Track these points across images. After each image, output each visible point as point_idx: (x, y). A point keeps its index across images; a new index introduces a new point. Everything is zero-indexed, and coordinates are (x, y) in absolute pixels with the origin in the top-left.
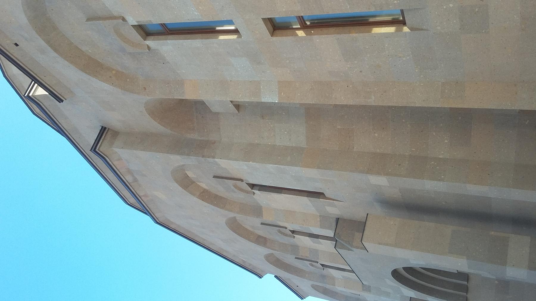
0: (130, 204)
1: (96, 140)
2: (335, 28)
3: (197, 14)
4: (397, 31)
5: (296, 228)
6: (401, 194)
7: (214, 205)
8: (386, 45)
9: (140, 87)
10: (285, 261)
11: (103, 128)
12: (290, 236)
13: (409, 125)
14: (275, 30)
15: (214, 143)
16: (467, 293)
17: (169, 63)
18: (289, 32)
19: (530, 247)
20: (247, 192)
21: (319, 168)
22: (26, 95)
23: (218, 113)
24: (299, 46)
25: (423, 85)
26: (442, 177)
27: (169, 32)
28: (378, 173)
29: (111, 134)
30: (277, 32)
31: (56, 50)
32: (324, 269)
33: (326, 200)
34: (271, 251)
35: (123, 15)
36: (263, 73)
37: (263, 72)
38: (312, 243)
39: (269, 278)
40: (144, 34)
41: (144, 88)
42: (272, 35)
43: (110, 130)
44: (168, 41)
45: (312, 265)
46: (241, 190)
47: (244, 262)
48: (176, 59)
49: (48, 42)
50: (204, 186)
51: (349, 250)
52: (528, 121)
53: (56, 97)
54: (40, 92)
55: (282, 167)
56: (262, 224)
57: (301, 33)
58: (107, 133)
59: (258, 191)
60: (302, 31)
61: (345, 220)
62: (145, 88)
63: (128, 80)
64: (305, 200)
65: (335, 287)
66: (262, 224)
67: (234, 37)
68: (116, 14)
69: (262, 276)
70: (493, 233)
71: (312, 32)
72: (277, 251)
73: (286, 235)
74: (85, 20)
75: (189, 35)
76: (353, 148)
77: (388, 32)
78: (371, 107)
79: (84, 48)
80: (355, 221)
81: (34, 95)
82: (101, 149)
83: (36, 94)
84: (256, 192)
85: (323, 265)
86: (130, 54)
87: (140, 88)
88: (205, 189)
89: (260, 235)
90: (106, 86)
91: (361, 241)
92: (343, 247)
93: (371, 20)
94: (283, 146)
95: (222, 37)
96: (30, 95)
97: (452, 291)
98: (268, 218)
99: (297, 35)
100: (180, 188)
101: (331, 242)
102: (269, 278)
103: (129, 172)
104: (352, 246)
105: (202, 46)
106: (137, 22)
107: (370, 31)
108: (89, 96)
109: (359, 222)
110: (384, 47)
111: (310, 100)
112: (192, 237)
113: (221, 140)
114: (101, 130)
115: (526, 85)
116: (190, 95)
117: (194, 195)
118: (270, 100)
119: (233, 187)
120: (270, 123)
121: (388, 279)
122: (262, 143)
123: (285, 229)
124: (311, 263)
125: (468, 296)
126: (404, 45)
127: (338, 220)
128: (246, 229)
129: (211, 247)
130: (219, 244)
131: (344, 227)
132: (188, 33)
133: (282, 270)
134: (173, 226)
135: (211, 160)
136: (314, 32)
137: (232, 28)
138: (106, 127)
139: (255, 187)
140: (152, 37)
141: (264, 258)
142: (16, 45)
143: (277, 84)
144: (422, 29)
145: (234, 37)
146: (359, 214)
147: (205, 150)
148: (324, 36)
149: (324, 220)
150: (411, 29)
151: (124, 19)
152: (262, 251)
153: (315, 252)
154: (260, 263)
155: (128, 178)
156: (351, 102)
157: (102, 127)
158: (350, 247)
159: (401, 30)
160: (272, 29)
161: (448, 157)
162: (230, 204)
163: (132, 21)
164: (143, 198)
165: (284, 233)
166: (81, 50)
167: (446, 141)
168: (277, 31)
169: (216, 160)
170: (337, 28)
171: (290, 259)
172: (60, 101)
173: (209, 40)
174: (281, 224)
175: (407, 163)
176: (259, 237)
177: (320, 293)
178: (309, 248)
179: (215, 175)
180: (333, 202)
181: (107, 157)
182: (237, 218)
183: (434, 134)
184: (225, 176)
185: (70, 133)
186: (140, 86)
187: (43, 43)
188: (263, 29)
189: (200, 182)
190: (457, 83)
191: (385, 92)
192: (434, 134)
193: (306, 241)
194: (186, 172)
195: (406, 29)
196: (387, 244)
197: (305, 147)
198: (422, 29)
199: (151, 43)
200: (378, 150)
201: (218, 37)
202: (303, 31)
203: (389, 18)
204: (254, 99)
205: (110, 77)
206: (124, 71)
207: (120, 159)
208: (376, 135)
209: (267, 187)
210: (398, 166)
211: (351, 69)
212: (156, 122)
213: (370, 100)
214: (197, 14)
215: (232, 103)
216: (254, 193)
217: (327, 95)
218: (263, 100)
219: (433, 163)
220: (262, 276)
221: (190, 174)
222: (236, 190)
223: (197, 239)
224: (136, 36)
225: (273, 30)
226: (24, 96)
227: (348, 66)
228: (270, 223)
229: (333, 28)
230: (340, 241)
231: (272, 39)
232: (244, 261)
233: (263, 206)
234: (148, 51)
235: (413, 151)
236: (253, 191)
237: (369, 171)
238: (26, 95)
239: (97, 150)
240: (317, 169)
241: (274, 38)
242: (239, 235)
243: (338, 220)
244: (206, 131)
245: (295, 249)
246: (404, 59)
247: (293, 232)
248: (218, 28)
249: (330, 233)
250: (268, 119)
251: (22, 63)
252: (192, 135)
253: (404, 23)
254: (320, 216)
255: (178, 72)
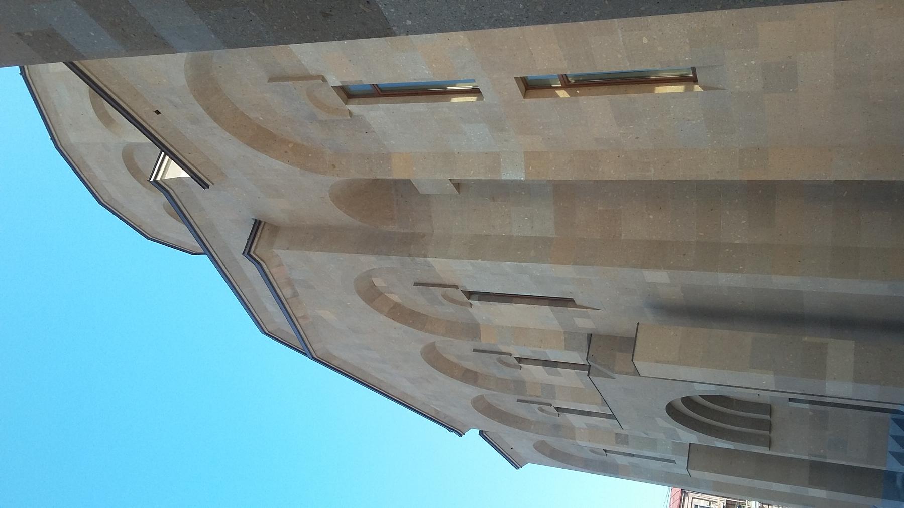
0: (267, 333)
1: (248, 240)
2: (607, 87)
3: (427, 73)
4: (686, 90)
5: (527, 352)
6: (683, 294)
7: (410, 325)
8: (672, 107)
9: (327, 164)
10: (500, 408)
11: (258, 222)
12: (515, 366)
13: (694, 203)
14: (529, 89)
15: (424, 236)
16: (770, 431)
17: (375, 133)
18: (546, 91)
19: (855, 354)
20: (461, 304)
21: (576, 264)
22: (152, 179)
23: (429, 195)
24: (559, 109)
25: (716, 153)
26: (741, 267)
27: (381, 94)
28: (657, 267)
29: (269, 230)
30: (531, 92)
31: (216, 119)
32: (559, 414)
33: (577, 309)
34: (483, 392)
35: (323, 74)
36: (505, 143)
37: (505, 141)
38: (547, 375)
39: (473, 434)
40: (345, 96)
41: (333, 165)
42: (525, 97)
43: (266, 225)
44: (379, 105)
45: (542, 410)
46: (453, 301)
47: (438, 412)
48: (386, 127)
49: (207, 109)
50: (395, 298)
51: (608, 378)
52: (846, 192)
53: (201, 182)
54: (173, 171)
55: (524, 264)
56: (475, 350)
57: (562, 94)
58: (263, 228)
59: (477, 302)
60: (564, 91)
61: (600, 336)
62: (334, 166)
63: (310, 155)
64: (545, 310)
65: (574, 441)
66: (475, 350)
67: (473, 99)
68: (313, 72)
69: (462, 433)
70: (806, 338)
71: (578, 92)
72: (494, 391)
73: (509, 365)
74: (267, 81)
75: (410, 97)
76: (621, 235)
77: (675, 92)
78: (651, 182)
79: (252, 115)
80: (615, 337)
81: (163, 179)
82: (257, 253)
83: (165, 178)
84: (475, 303)
85: (558, 409)
86: (321, 121)
87: (327, 166)
88: (396, 303)
89: (468, 368)
90: (278, 165)
91: (632, 360)
92: (600, 374)
93: (653, 77)
94: (523, 236)
95: (455, 100)
96: (158, 178)
97: (750, 430)
98: (485, 341)
99: (558, 96)
100: (363, 303)
101: (576, 372)
102: (473, 434)
103: (290, 283)
104: (613, 371)
105: (427, 110)
106: (341, 82)
107: (652, 91)
108: (248, 179)
109: (621, 337)
110: (669, 108)
111: (568, 174)
112: (359, 375)
113: (433, 231)
114: (254, 225)
115: (842, 150)
116: (398, 173)
117: (381, 312)
118: (514, 177)
119: (441, 298)
120: (504, 206)
121: (661, 418)
122: (492, 234)
123: (509, 356)
124: (541, 407)
125: (772, 435)
126: (694, 106)
127: (590, 337)
128: (449, 360)
129: (391, 391)
130: (405, 387)
131: (600, 346)
132: (408, 95)
133: (496, 421)
134: (335, 363)
135: (422, 259)
136: (579, 92)
137: (469, 87)
138: (261, 220)
139: (473, 297)
140: (356, 100)
141: (471, 404)
142: (158, 112)
143: (523, 156)
144: (717, 89)
145: (471, 99)
146: (623, 326)
147: (412, 246)
148: (593, 97)
149: (570, 338)
150: (704, 88)
151: (324, 80)
152: (471, 391)
153: (550, 389)
154: (454, 413)
155: (286, 293)
156: (623, 177)
157: (256, 220)
158: (609, 373)
159: (692, 90)
160: (524, 88)
161: (747, 242)
162: (432, 322)
163: (334, 80)
164: (300, 321)
165: (506, 363)
166: (249, 118)
167: (744, 222)
168: (531, 90)
169: (429, 259)
170: (610, 87)
171: (508, 402)
172: (205, 185)
173: (438, 103)
174: (504, 348)
175: (694, 252)
176: (467, 371)
177: (546, 456)
178: (541, 384)
179: (417, 281)
180: (587, 311)
181: (264, 261)
182: (438, 345)
183: (728, 213)
184: (432, 282)
185: (203, 231)
186: (328, 163)
187: (200, 110)
188: (515, 89)
189: (391, 293)
190: (759, 149)
191: (668, 162)
192: (728, 213)
193: (538, 373)
194: (374, 279)
195: (697, 88)
196: (668, 362)
197: (554, 236)
198: (717, 89)
199: (354, 107)
200: (654, 237)
201: (450, 100)
202: (566, 91)
203: (675, 75)
204: (490, 176)
205: (286, 152)
206: (305, 143)
207: (280, 265)
208: (651, 217)
209: (490, 295)
210: (682, 256)
211: (624, 135)
212: (341, 211)
213: (648, 174)
214: (427, 73)
215: (451, 181)
216: (471, 305)
217: (592, 168)
218: (504, 178)
219: (727, 250)
220: (462, 433)
221: (378, 282)
222: (446, 302)
223: (370, 380)
224: (336, 100)
225: (525, 90)
226: (149, 181)
227: (621, 131)
228: (487, 349)
229: (604, 87)
230: (597, 366)
231: (524, 101)
232: (438, 410)
233: (481, 324)
234: (349, 118)
235: (701, 235)
236: (470, 301)
237: (645, 265)
238: (152, 179)
239: (251, 253)
240: (573, 266)
241: (527, 101)
242: (437, 368)
243: (590, 337)
244: (411, 220)
245: (519, 386)
246: (694, 122)
247: (520, 360)
248: (449, 88)
249: (577, 357)
250: (501, 201)
251: (161, 136)
252: (390, 226)
253: (694, 80)
254: (565, 333)
255: (385, 143)
